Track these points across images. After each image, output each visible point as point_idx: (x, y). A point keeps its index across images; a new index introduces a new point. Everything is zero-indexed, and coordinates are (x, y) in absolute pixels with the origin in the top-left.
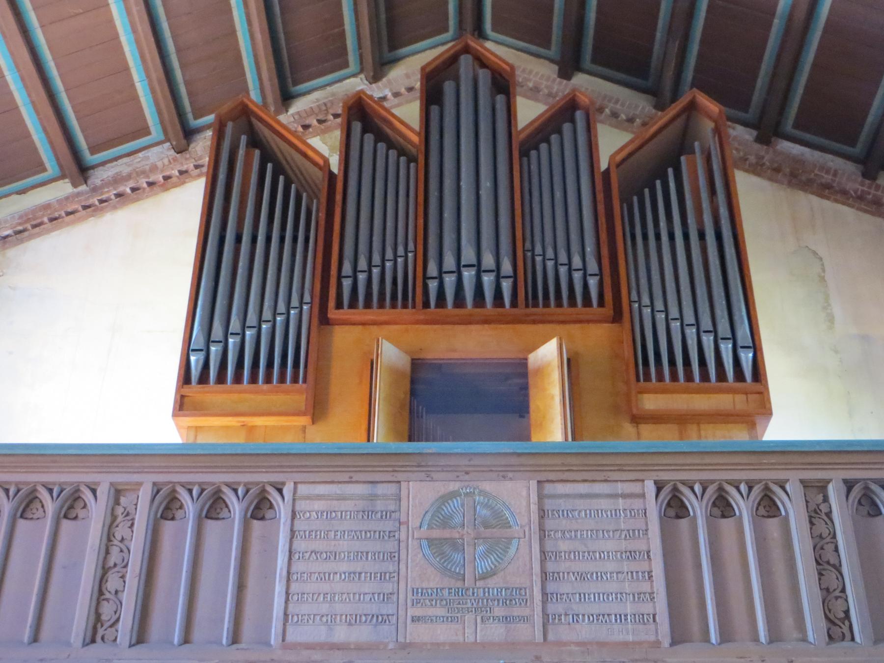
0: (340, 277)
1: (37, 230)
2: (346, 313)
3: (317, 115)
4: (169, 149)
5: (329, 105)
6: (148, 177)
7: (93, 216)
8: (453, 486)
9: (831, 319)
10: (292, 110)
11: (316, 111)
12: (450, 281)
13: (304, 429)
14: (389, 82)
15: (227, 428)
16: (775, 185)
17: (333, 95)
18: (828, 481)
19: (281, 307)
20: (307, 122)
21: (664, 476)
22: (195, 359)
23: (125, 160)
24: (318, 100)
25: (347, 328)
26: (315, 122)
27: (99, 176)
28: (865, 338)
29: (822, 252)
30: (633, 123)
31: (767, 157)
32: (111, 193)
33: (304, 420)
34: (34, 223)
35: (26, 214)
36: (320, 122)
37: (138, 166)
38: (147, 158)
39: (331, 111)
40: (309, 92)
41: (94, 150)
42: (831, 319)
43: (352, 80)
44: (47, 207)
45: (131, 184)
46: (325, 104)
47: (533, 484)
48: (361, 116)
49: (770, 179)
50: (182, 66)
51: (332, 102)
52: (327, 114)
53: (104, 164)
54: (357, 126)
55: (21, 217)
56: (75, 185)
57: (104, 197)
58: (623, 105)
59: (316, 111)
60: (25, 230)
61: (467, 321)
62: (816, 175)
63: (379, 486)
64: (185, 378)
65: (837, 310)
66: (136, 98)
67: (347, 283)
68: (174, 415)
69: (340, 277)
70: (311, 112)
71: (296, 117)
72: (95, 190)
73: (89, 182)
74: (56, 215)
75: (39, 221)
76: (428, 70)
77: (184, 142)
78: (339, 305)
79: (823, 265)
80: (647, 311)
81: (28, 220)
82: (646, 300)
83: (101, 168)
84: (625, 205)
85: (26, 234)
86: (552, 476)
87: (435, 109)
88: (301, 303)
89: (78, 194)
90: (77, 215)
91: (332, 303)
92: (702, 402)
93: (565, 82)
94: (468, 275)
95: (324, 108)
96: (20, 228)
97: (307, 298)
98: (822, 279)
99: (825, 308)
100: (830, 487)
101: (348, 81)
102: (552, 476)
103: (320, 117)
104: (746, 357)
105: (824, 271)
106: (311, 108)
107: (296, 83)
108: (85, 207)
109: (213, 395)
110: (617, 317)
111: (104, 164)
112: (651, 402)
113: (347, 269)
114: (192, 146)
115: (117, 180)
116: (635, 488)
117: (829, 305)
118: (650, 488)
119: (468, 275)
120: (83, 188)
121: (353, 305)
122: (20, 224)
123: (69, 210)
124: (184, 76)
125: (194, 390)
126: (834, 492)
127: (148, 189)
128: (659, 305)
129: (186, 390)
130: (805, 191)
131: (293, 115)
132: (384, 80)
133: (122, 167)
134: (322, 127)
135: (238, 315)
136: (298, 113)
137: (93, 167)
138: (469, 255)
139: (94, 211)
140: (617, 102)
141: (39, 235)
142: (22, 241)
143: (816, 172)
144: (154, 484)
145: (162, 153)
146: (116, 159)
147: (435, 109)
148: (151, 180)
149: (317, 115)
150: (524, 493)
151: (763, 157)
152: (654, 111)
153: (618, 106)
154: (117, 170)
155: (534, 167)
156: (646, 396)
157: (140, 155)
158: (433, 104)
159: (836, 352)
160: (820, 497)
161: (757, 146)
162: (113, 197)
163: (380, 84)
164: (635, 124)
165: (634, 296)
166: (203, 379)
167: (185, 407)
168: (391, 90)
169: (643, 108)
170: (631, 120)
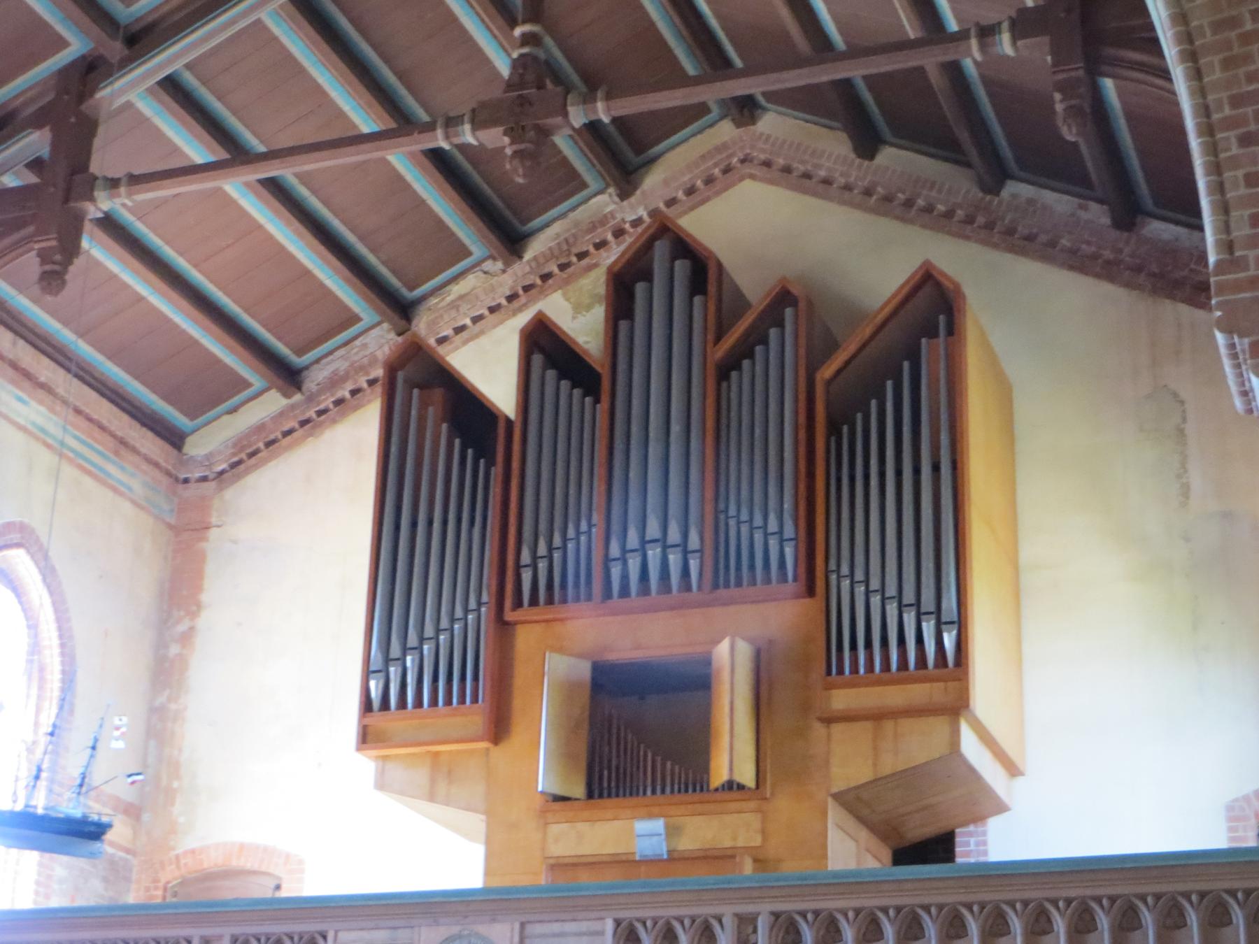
0: (518, 567)
1: (253, 461)
2: (525, 613)
3: (557, 258)
4: (389, 331)
5: (571, 240)
6: (367, 374)
7: (311, 435)
8: (455, 930)
9: (1186, 491)
10: (528, 256)
11: (556, 252)
12: (634, 564)
13: (487, 749)
14: (643, 193)
15: (414, 754)
16: (1135, 293)
17: (577, 224)
18: (759, 914)
19: (459, 613)
20: (546, 270)
21: (621, 915)
22: (375, 687)
23: (342, 352)
24: (558, 235)
25: (527, 625)
26: (556, 270)
27: (316, 378)
28: (1227, 516)
29: (1183, 395)
30: (952, 217)
31: (1127, 250)
32: (327, 402)
33: (484, 745)
34: (249, 450)
35: (240, 440)
36: (563, 267)
37: (356, 358)
38: (365, 346)
39: (575, 250)
40: (547, 225)
41: (300, 352)
42: (1186, 491)
43: (599, 198)
44: (260, 428)
45: (350, 386)
46: (566, 240)
47: (517, 926)
48: (543, 344)
49: (1128, 285)
50: (373, 251)
51: (574, 236)
52: (569, 255)
53: (317, 361)
54: (537, 359)
55: (235, 445)
56: (287, 395)
57: (322, 407)
58: (940, 191)
59: (556, 252)
60: (239, 462)
61: (655, 609)
62: (1191, 270)
63: (400, 931)
64: (367, 706)
65: (1196, 478)
66: (327, 293)
67: (527, 576)
68: (358, 749)
69: (518, 567)
70: (550, 255)
71: (533, 264)
72: (311, 399)
73: (304, 388)
74: (272, 437)
75: (254, 447)
76: (616, 269)
77: (403, 322)
78: (518, 604)
79: (1184, 411)
80: (846, 584)
81: (242, 449)
82: (845, 570)
83: (316, 366)
84: (833, 439)
85: (242, 467)
86: (532, 918)
87: (623, 325)
88: (479, 604)
89: (292, 407)
90: (295, 435)
91: (508, 603)
92: (894, 696)
93: (866, 163)
94: (654, 553)
95: (565, 247)
96: (235, 459)
97: (485, 598)
98: (1181, 432)
99: (1179, 476)
100: (760, 919)
101: (594, 200)
102: (532, 918)
103: (563, 260)
104: (949, 640)
105: (1184, 420)
106: (550, 249)
107: (525, 222)
108: (304, 423)
109: (392, 722)
110: (810, 591)
111: (317, 361)
112: (841, 699)
113: (526, 557)
114: (414, 323)
115: (335, 381)
116: (595, 926)
117: (1186, 471)
118: (609, 925)
119: (654, 553)
120: (298, 397)
121: (534, 602)
122: (234, 455)
123: (286, 428)
124: (378, 258)
125: (377, 719)
126: (763, 924)
127: (369, 391)
128: (859, 576)
129: (368, 721)
130: (1172, 297)
131: (528, 262)
132: (638, 192)
133: (337, 364)
134: (564, 275)
135: (415, 626)
136: (535, 258)
137: (307, 368)
138: (653, 530)
139: (314, 428)
140: (932, 188)
141: (256, 467)
142: (239, 477)
143: (1193, 266)
144: (232, 936)
145: (382, 337)
146: (331, 353)
147: (623, 325)
148: (371, 377)
149: (557, 258)
150: (509, 934)
151: (1120, 251)
152: (981, 195)
153: (934, 194)
154: (331, 368)
155: (734, 395)
156: (835, 692)
157: (357, 342)
158: (623, 319)
159: (1187, 540)
160: (750, 930)
161: (1114, 234)
162: (331, 406)
163: (633, 199)
164: (956, 219)
165: (833, 566)
166: (385, 705)
167: (369, 738)
168: (646, 208)
169: (968, 192)
170: (949, 214)
